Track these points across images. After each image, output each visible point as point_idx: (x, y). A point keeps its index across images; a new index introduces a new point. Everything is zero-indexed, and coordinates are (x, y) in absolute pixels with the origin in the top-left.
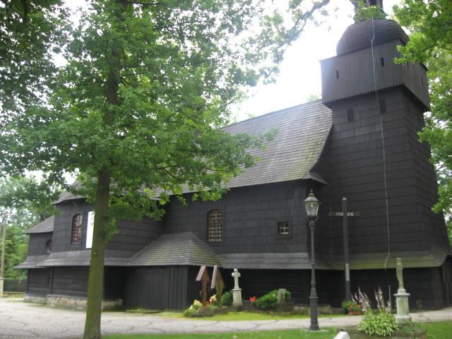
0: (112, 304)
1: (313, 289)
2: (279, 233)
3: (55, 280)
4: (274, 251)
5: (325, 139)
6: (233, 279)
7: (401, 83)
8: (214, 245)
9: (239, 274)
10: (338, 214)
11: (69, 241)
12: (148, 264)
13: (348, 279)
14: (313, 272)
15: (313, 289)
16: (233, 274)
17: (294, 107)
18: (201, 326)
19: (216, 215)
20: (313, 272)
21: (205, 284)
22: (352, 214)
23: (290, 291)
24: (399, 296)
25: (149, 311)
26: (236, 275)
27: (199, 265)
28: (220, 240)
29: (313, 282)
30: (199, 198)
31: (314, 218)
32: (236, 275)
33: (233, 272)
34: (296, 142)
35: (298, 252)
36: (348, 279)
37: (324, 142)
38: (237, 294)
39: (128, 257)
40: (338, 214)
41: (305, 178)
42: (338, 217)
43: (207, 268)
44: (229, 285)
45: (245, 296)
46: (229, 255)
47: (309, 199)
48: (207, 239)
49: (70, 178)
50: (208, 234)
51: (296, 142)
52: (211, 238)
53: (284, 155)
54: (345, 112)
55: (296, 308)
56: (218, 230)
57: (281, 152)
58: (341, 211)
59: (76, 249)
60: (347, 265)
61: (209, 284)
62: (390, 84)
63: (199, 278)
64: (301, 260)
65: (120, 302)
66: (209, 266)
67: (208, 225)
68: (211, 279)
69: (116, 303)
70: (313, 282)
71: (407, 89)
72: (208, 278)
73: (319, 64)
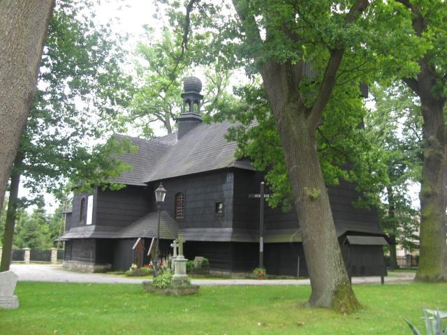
0: (102, 267)
3: (73, 249)
4: (213, 227)
8: (178, 221)
10: (256, 196)
11: (79, 220)
12: (123, 237)
13: (261, 250)
18: (86, 271)
19: (181, 197)
23: (208, 258)
28: (182, 218)
30: (108, 189)
33: (173, 243)
36: (261, 250)
39: (115, 231)
40: (256, 196)
46: (188, 230)
48: (175, 217)
50: (175, 212)
55: (211, 272)
58: (259, 193)
59: (82, 226)
60: (261, 239)
64: (224, 234)
65: (109, 266)
67: (176, 204)
69: (106, 266)
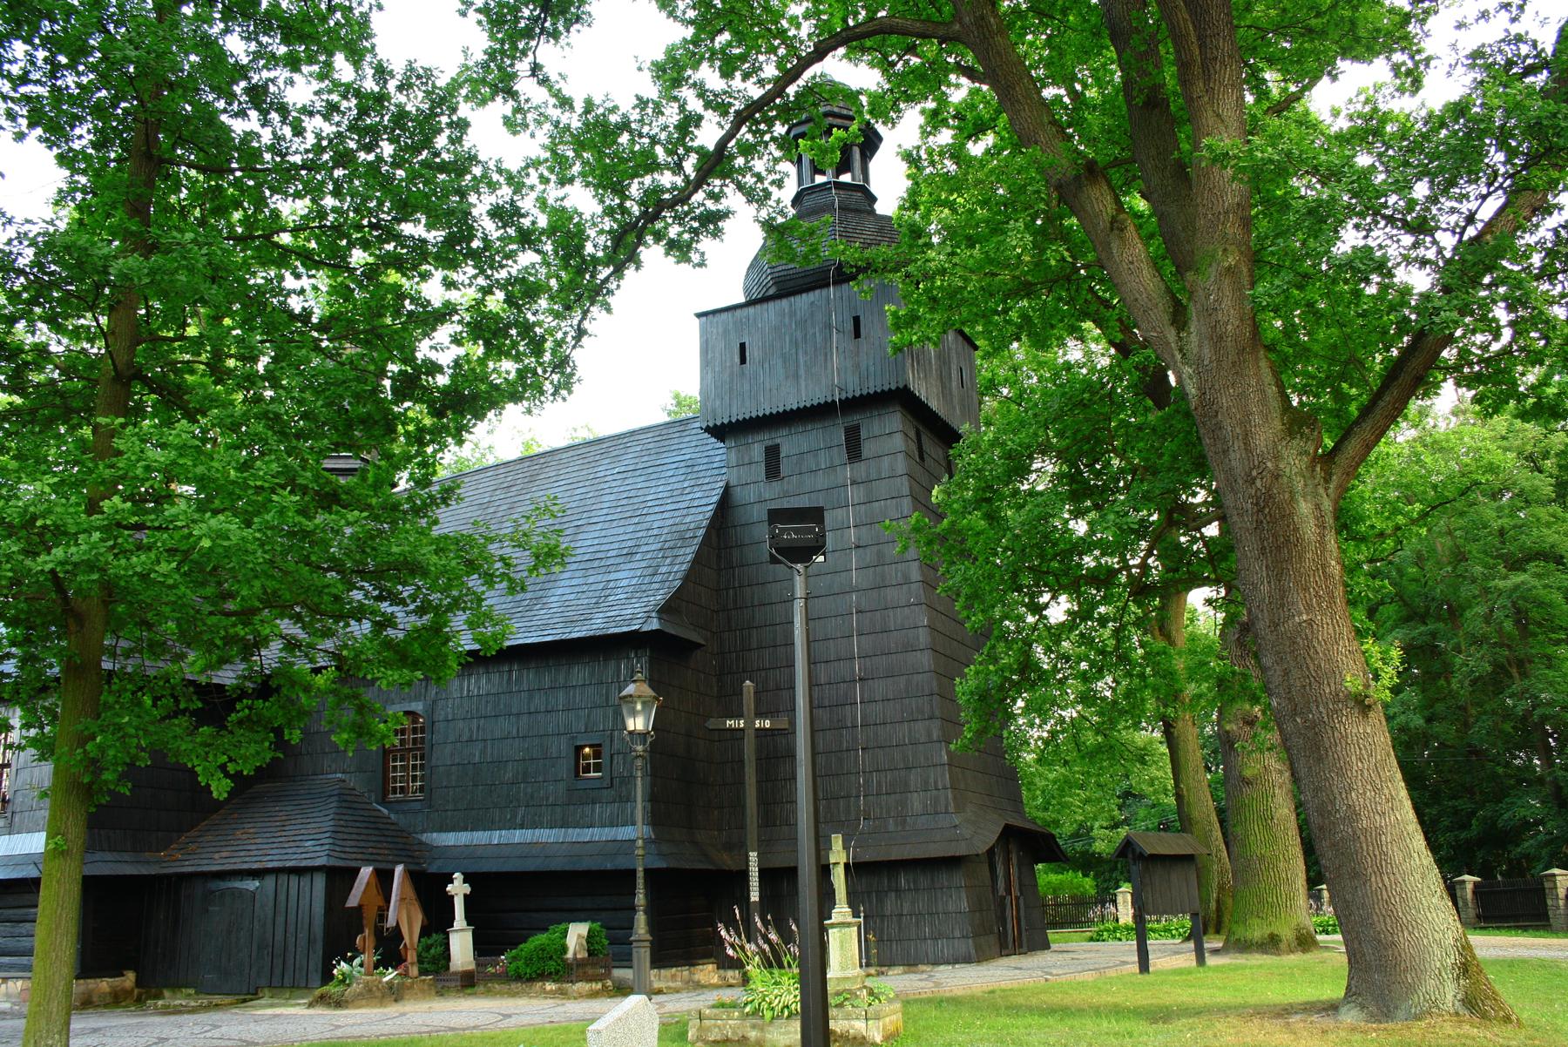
1: (641, 919)
2: (577, 774)
5: (705, 523)
6: (450, 900)
7: (901, 386)
9: (467, 889)
14: (640, 875)
15: (641, 919)
16: (450, 887)
17: (632, 433)
20: (640, 875)
21: (370, 916)
22: (768, 724)
24: (833, 926)
25: (217, 999)
26: (458, 889)
27: (354, 864)
29: (640, 899)
31: (643, 736)
32: (458, 889)
34: (631, 529)
35: (454, 829)
37: (701, 532)
38: (461, 945)
41: (646, 628)
42: (731, 730)
43: (377, 872)
44: (438, 919)
45: (482, 947)
47: (631, 689)
48: (385, 793)
49: (1488, 141)
51: (631, 529)
52: (394, 791)
53: (596, 564)
54: (840, 437)
56: (414, 767)
57: (587, 557)
58: (739, 716)
60: (753, 856)
61: (382, 917)
62: (874, 386)
63: (353, 901)
66: (382, 866)
68: (388, 901)
69: (117, 981)
70: (640, 899)
71: (918, 400)
72: (380, 902)
73: (690, 336)
